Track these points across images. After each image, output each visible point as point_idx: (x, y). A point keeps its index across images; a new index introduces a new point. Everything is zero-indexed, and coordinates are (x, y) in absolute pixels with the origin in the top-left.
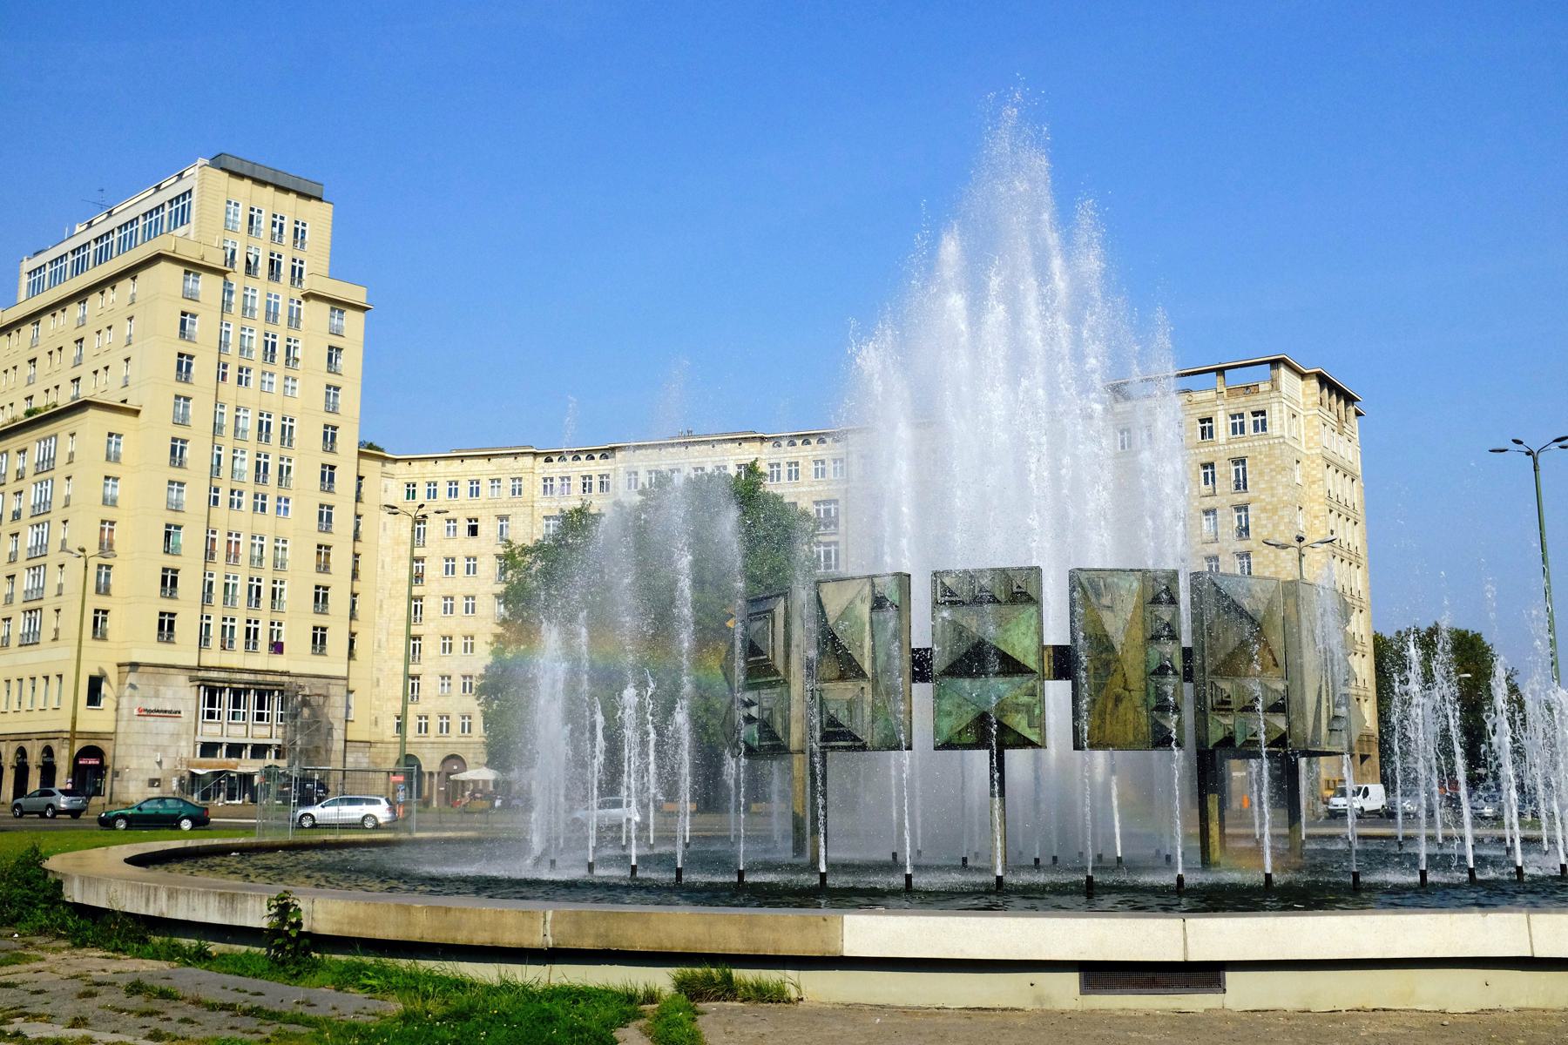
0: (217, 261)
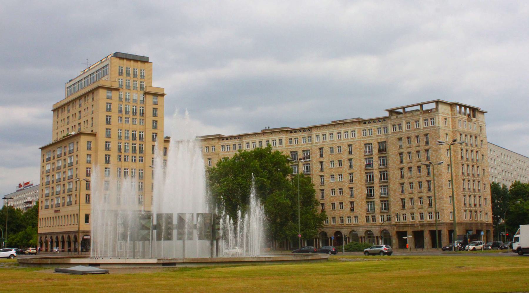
0: (116, 85)
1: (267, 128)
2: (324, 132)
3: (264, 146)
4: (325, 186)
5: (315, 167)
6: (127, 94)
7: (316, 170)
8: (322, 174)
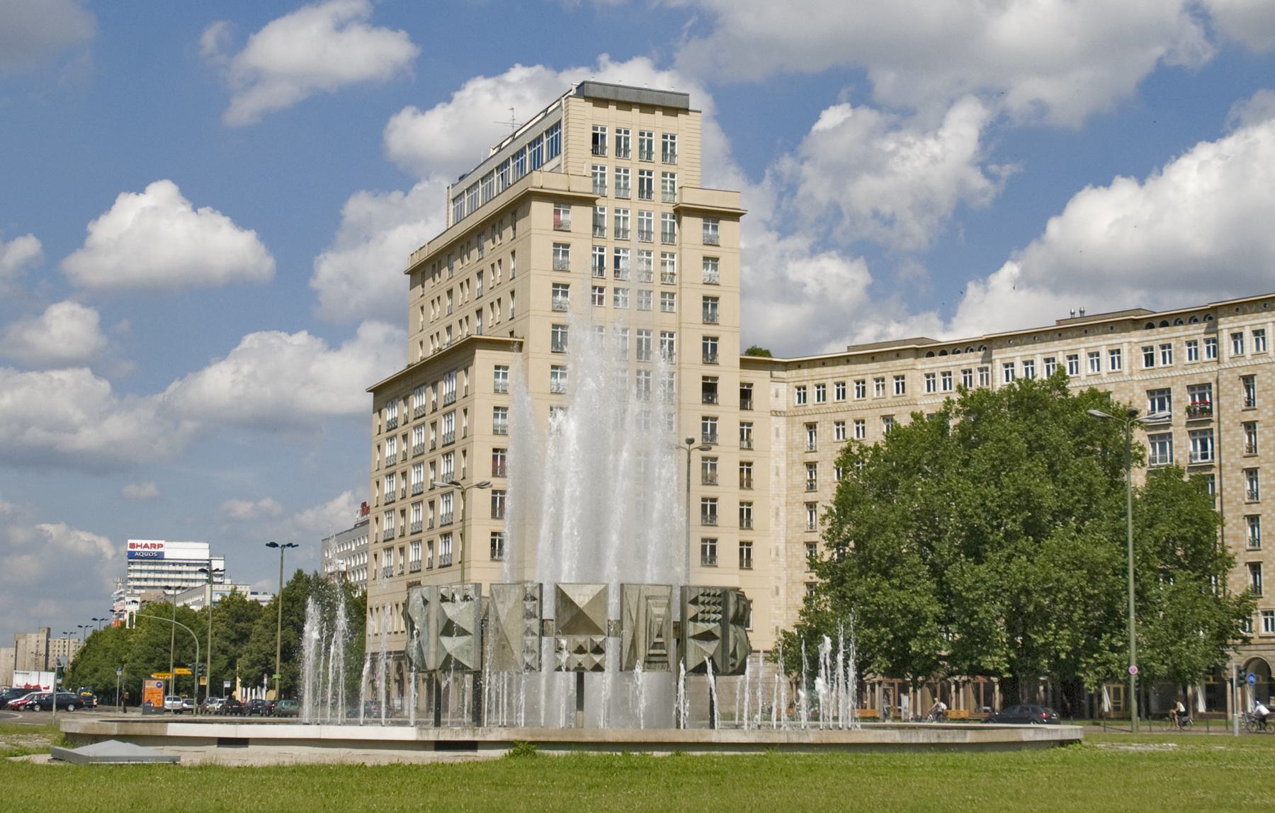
0: (583, 187)
1: (1078, 315)
2: (1257, 321)
3: (1041, 374)
4: (1264, 504)
5: (1228, 439)
6: (621, 214)
7: (1233, 450)
8: (1251, 463)
